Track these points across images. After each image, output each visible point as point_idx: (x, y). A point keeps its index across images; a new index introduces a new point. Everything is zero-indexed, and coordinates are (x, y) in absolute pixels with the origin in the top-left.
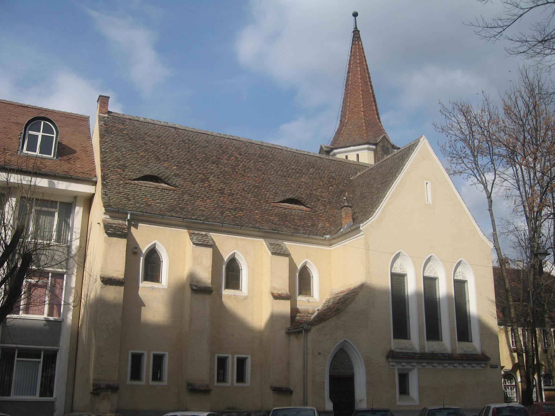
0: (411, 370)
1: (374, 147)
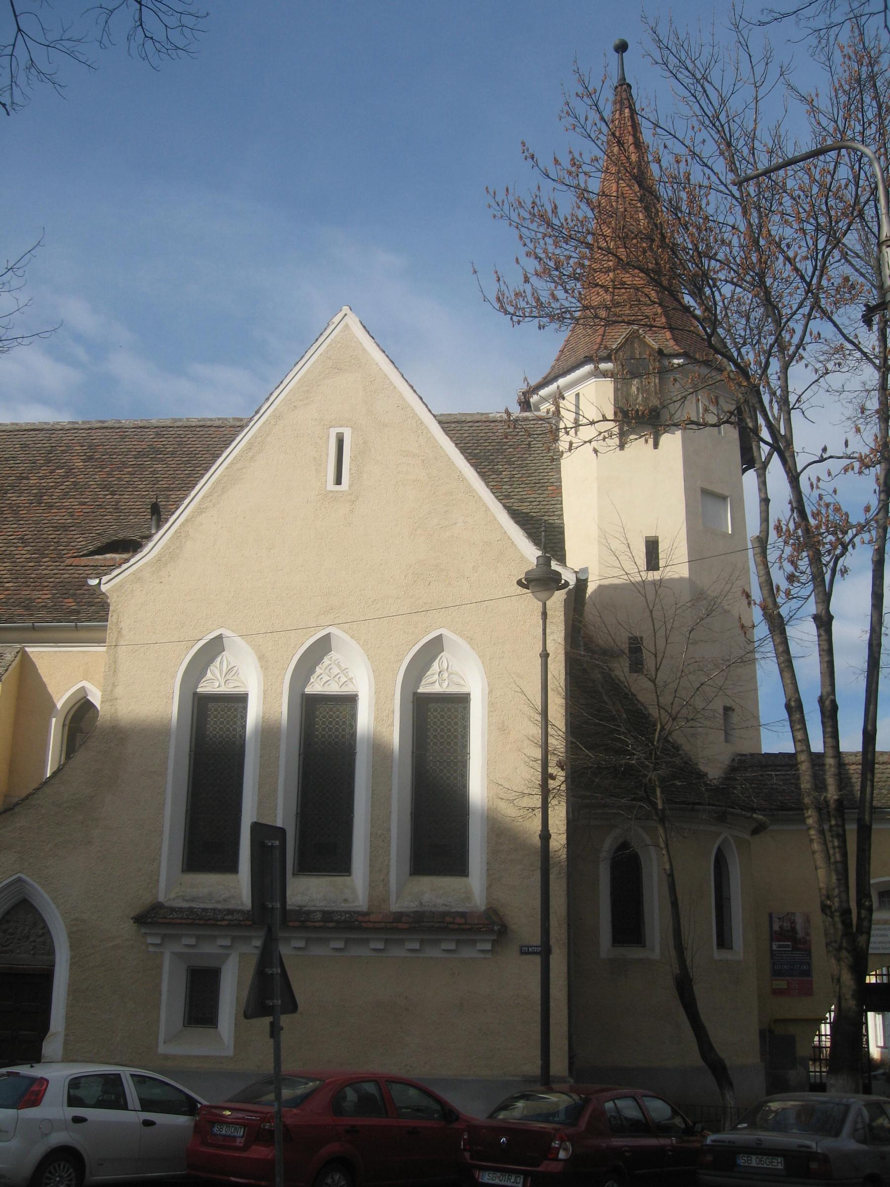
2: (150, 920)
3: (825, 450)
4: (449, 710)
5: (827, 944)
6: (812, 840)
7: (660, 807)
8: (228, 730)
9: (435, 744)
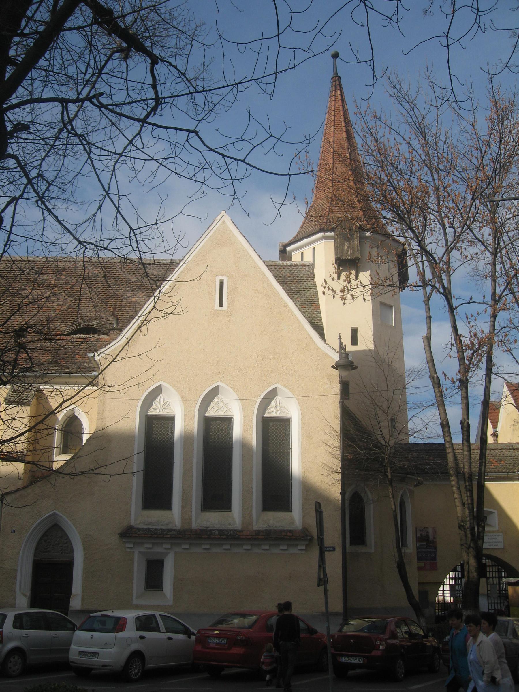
0: (167, 554)
1: (332, 234)
2: (128, 535)
3: (471, 298)
4: (280, 426)
5: (462, 545)
6: (454, 493)
7: (390, 477)
8: (164, 435)
9: (273, 443)
